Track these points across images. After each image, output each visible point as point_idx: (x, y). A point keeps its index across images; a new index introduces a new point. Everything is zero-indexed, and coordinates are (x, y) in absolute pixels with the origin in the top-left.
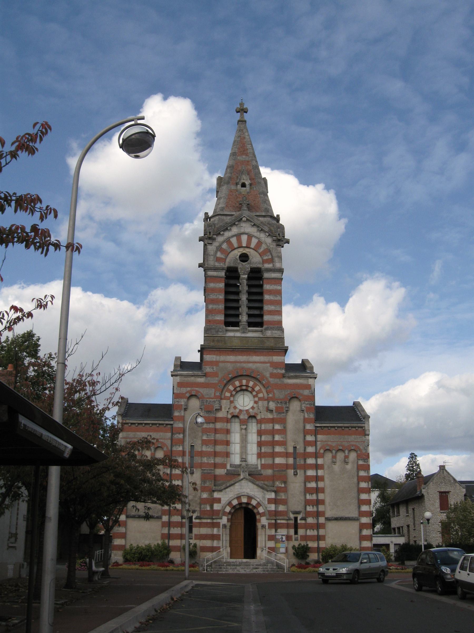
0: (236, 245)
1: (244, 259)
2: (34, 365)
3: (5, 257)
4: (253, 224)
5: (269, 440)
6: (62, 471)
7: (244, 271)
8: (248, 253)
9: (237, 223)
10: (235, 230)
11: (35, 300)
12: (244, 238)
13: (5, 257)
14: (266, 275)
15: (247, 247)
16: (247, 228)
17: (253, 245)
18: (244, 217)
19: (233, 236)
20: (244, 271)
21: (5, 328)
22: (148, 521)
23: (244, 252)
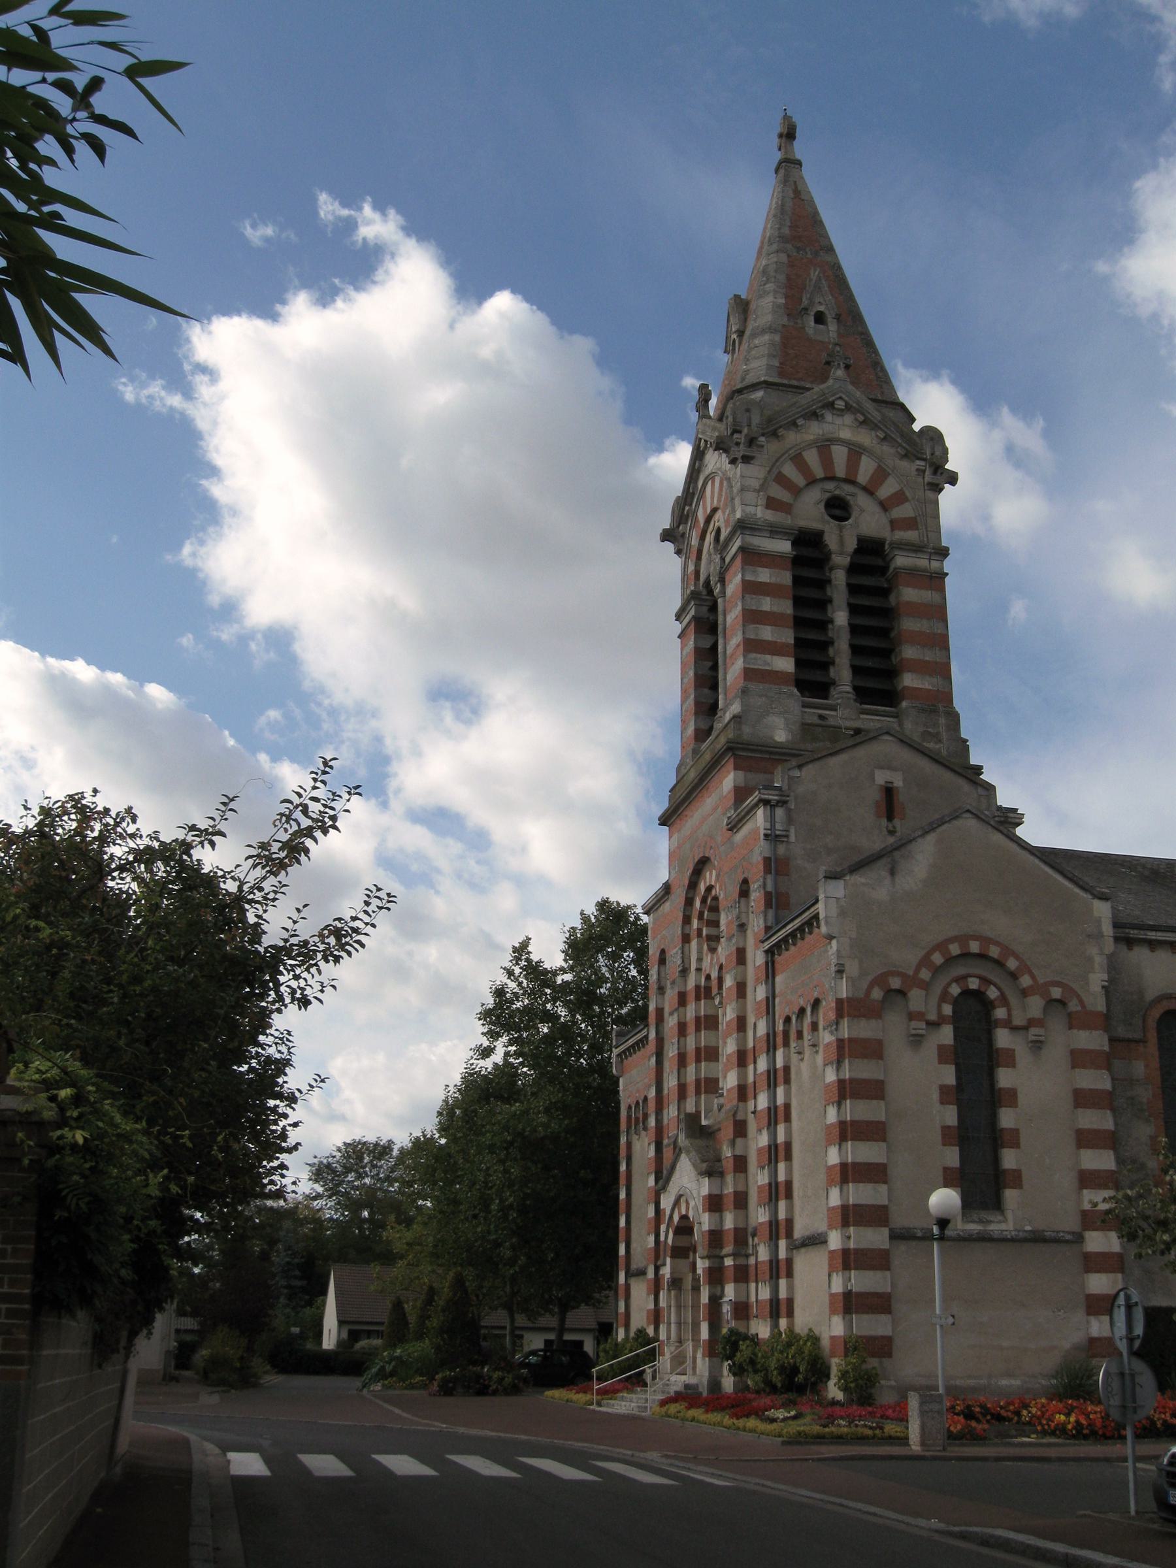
0: (800, 480)
1: (837, 512)
2: (286, 1287)
3: (91, 43)
4: (861, 418)
5: (1106, 1127)
6: (320, 1343)
7: (841, 544)
8: (849, 498)
9: (800, 422)
10: (815, 430)
11: (212, 823)
12: (840, 454)
13: (91, 43)
14: (901, 560)
15: (850, 481)
16: (843, 428)
17: (863, 477)
18: (840, 398)
19: (810, 445)
20: (841, 544)
21: (755, 1354)
22: (438, 1104)
23: (837, 492)
